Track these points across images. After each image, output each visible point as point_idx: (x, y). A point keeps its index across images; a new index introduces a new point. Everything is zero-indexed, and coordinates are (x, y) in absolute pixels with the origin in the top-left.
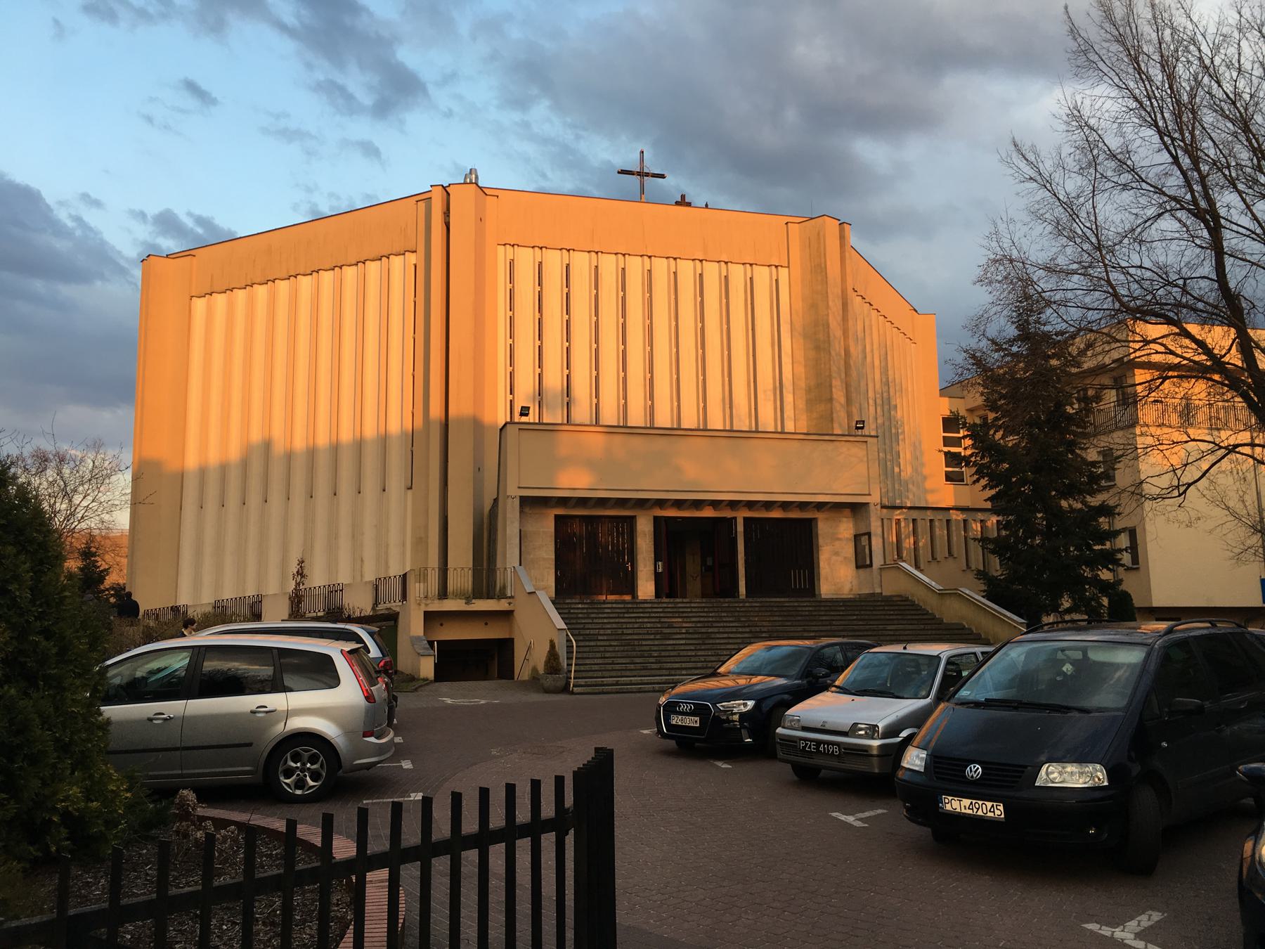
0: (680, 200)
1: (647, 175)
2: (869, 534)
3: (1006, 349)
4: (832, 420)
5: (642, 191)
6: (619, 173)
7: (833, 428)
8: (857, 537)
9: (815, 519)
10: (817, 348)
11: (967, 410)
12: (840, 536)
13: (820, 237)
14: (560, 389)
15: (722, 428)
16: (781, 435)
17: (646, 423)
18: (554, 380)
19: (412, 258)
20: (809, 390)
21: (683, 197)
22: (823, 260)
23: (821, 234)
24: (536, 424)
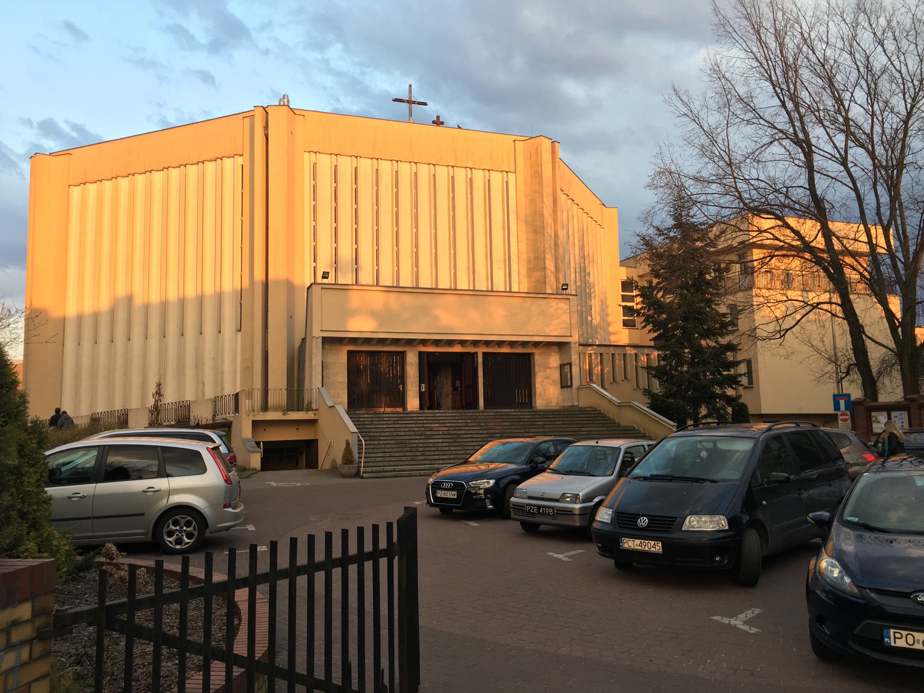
1: (414, 102)
2: (570, 364)
3: (666, 234)
6: (393, 100)
7: (545, 289)
8: (562, 366)
9: (533, 353)
10: (535, 232)
12: (551, 366)
13: (538, 151)
20: (529, 262)
21: (438, 117)
22: (540, 169)
23: (539, 149)
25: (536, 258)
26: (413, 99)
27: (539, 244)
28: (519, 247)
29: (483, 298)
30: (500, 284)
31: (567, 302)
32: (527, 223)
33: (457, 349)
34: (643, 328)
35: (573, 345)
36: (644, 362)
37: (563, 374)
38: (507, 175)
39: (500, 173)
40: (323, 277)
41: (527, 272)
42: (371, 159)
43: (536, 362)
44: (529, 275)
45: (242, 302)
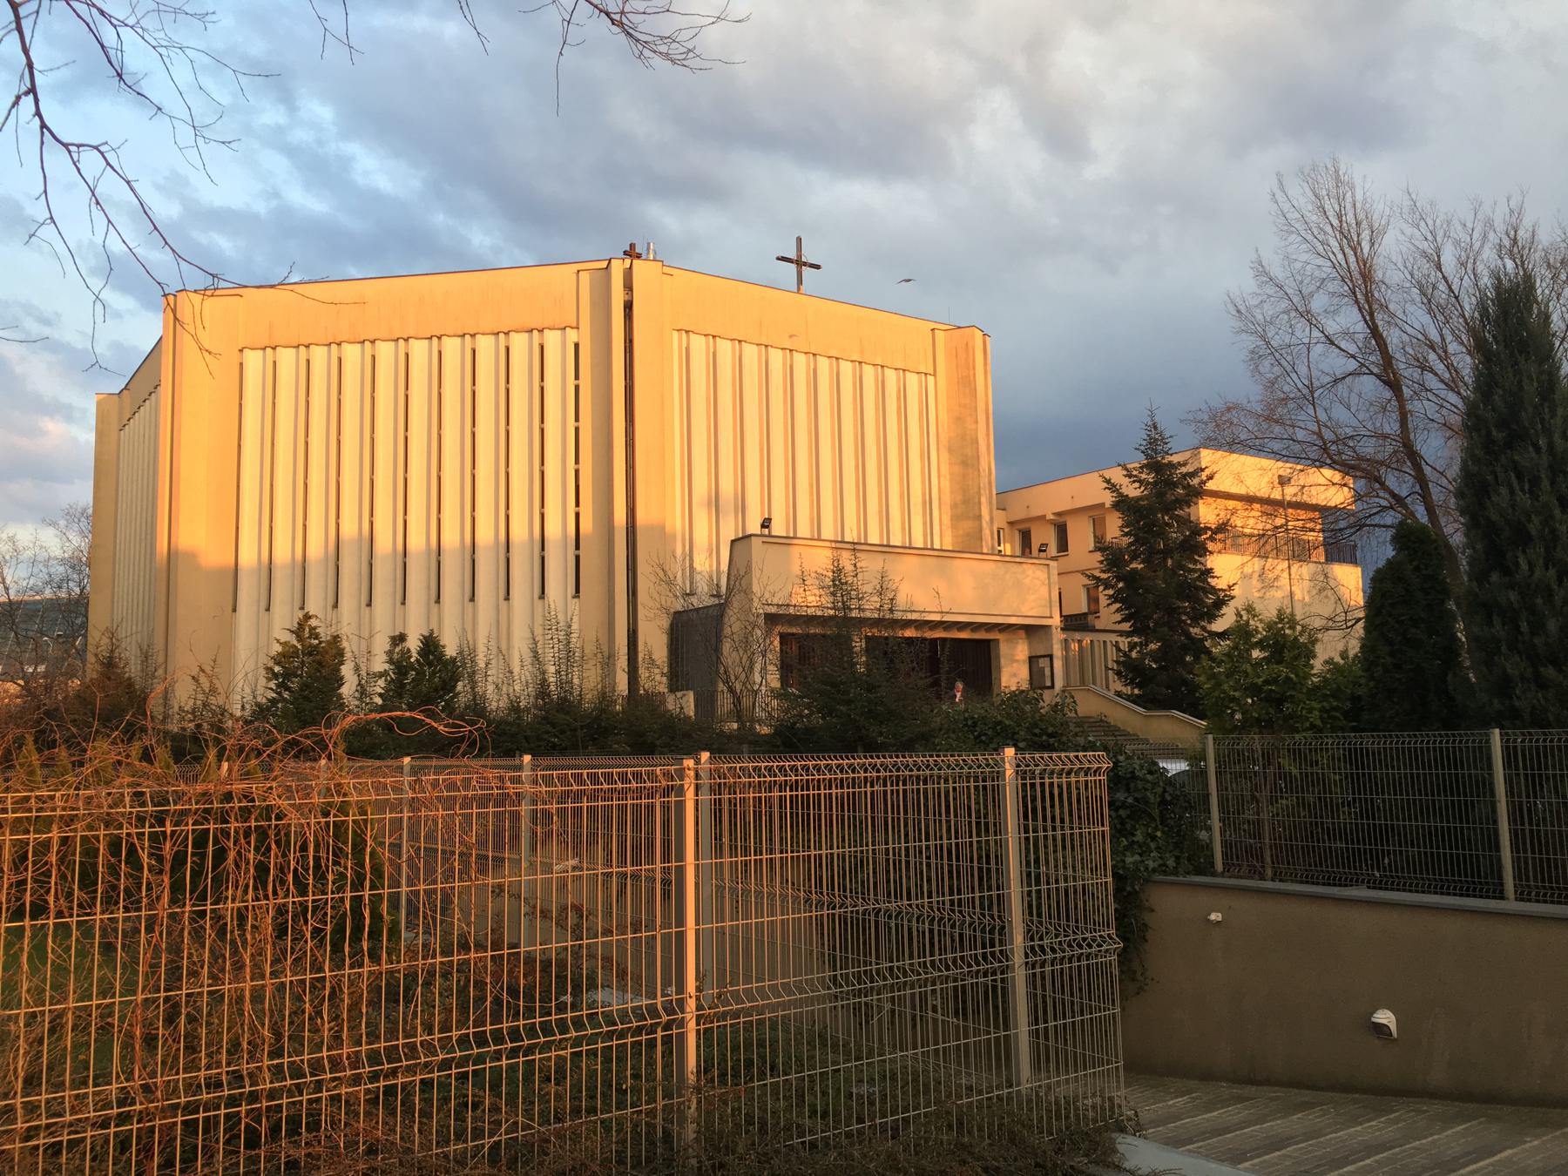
0: (628, 249)
1: (805, 264)
2: (1051, 657)
3: (1135, 476)
4: (982, 539)
5: (800, 281)
6: (778, 259)
7: (982, 547)
8: (1032, 660)
9: (997, 641)
10: (964, 463)
11: (1009, 523)
12: (1017, 658)
13: (968, 348)
14: (733, 492)
15: (878, 543)
16: (927, 551)
17: (788, 531)
18: (728, 487)
19: (572, 336)
20: (954, 506)
21: (632, 246)
22: (972, 373)
23: (970, 345)
24: (906, 548)
25: (966, 502)
26: (804, 259)
27: (970, 483)
28: (942, 486)
29: (949, 561)
30: (918, 542)
31: (1045, 568)
32: (950, 450)
33: (909, 633)
34: (1108, 605)
35: (1054, 630)
36: (1075, 651)
37: (1034, 669)
38: (904, 375)
39: (915, 375)
40: (1040, 551)
41: (951, 520)
42: (806, 353)
43: (1001, 653)
44: (954, 527)
45: (582, 553)
